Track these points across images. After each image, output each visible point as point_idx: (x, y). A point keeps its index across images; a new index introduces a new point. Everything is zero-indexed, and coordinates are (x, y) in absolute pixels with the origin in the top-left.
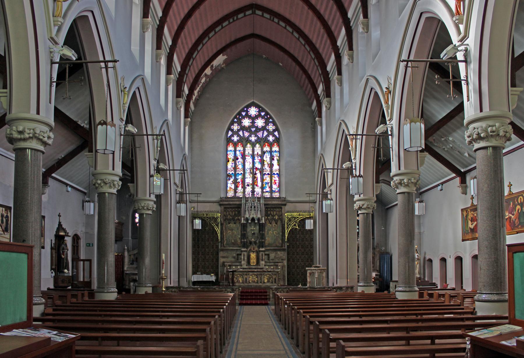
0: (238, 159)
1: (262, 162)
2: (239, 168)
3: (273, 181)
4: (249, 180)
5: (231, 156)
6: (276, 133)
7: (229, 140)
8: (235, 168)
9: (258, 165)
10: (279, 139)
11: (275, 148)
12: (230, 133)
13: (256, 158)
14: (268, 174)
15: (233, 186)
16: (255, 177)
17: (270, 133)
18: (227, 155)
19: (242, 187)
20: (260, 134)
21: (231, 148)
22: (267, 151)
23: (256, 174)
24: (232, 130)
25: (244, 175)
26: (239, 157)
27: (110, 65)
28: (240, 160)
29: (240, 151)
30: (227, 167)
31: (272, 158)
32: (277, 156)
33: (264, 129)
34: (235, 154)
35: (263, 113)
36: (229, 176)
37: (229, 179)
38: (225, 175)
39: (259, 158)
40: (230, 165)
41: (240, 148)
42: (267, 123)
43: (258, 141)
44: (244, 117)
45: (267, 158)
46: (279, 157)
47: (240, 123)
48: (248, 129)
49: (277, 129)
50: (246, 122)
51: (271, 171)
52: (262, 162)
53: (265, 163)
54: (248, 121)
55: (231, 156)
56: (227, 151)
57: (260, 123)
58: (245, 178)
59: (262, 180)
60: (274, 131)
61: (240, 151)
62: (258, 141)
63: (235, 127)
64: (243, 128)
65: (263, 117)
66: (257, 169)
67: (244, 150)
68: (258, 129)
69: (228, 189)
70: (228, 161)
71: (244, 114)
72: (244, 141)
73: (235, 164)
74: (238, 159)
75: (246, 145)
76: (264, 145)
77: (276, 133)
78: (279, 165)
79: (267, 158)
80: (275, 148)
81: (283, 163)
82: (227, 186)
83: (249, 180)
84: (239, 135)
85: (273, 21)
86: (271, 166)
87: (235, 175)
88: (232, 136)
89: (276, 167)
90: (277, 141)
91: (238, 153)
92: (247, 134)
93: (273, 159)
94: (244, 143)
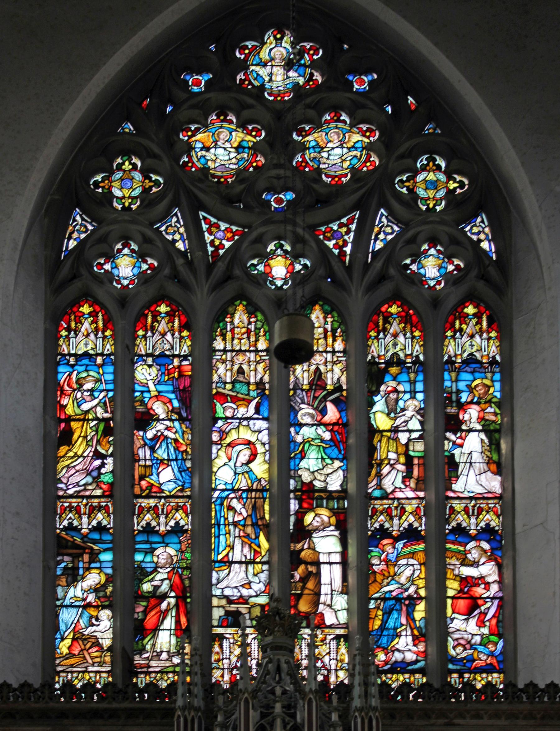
0: (146, 419)
1: (357, 444)
2: (154, 491)
3: (452, 587)
4: (242, 580)
5: (87, 399)
6: (479, 231)
7: (67, 285)
8: (126, 490)
9: (323, 470)
10: (503, 263)
11: (472, 341)
12: (80, 228)
13: (305, 413)
14: (411, 535)
15: (104, 628)
16: (296, 560)
17: (419, 229)
18: (53, 389)
19: (181, 632)
20: (340, 237)
21: (85, 338)
22: (396, 361)
23: (304, 533)
24: (98, 205)
25: (200, 539)
26: (159, 409)
27: (329, 349)
28: (165, 426)
29: (161, 359)
30: (50, 477)
31: (445, 419)
32: (483, 401)
33: (368, 192)
34: (125, 380)
35: (358, 65)
36: (66, 552)
37: (73, 576)
38: (35, 536)
39: (332, 413)
40: (76, 470)
41: (166, 337)
42: (398, 147)
43: (324, 283)
44: (201, 111)
45: (398, 414)
46: (505, 404)
47: (165, 149)
48: (237, 196)
49: (487, 195)
50: (221, 148)
51: (438, 507)
52: (357, 444)
53: (386, 451)
54: (238, 136)
55: (87, 399)
56: (53, 358)
57: (337, 149)
58: (209, 565)
59: (360, 580)
60: (462, 208)
61: (161, 359)
62: (324, 283)
63: (126, 187)
64: (193, 191)
65: (360, 111)
66: (310, 495)
67: (204, 357)
68: (319, 197)
69: (64, 647)
70: (66, 438)
71: (198, 82)
72: (202, 290)
73: (127, 459)
74: (146, 419)
75: (223, 313)
76: (375, 320)
77: (479, 231)
78: (497, 465)
79: (398, 414)
80: (472, 341)
81: (523, 449)
82: (51, 627)
83: (242, 580)
84: (150, 245)
85: (250, 652)
86: (437, 470)
87: (125, 541)
88: (101, 245)
89: (474, 481)
90: (490, 287)
91: (145, 374)
92: (220, 236)
93: (455, 425)
94: (202, 300)
